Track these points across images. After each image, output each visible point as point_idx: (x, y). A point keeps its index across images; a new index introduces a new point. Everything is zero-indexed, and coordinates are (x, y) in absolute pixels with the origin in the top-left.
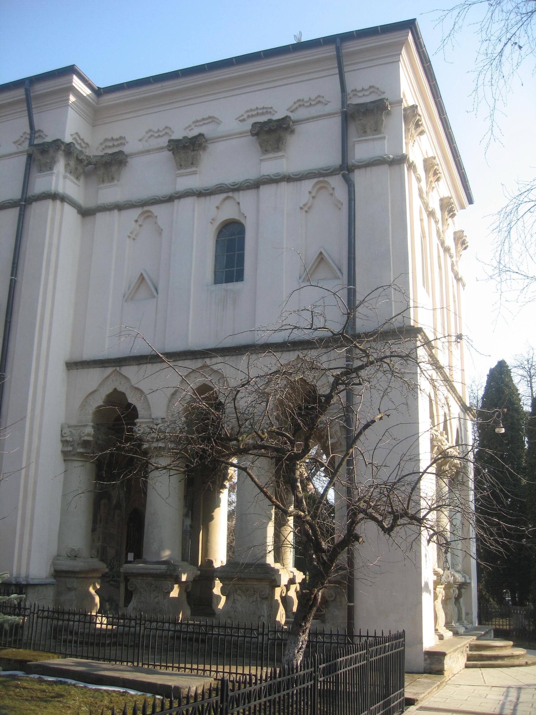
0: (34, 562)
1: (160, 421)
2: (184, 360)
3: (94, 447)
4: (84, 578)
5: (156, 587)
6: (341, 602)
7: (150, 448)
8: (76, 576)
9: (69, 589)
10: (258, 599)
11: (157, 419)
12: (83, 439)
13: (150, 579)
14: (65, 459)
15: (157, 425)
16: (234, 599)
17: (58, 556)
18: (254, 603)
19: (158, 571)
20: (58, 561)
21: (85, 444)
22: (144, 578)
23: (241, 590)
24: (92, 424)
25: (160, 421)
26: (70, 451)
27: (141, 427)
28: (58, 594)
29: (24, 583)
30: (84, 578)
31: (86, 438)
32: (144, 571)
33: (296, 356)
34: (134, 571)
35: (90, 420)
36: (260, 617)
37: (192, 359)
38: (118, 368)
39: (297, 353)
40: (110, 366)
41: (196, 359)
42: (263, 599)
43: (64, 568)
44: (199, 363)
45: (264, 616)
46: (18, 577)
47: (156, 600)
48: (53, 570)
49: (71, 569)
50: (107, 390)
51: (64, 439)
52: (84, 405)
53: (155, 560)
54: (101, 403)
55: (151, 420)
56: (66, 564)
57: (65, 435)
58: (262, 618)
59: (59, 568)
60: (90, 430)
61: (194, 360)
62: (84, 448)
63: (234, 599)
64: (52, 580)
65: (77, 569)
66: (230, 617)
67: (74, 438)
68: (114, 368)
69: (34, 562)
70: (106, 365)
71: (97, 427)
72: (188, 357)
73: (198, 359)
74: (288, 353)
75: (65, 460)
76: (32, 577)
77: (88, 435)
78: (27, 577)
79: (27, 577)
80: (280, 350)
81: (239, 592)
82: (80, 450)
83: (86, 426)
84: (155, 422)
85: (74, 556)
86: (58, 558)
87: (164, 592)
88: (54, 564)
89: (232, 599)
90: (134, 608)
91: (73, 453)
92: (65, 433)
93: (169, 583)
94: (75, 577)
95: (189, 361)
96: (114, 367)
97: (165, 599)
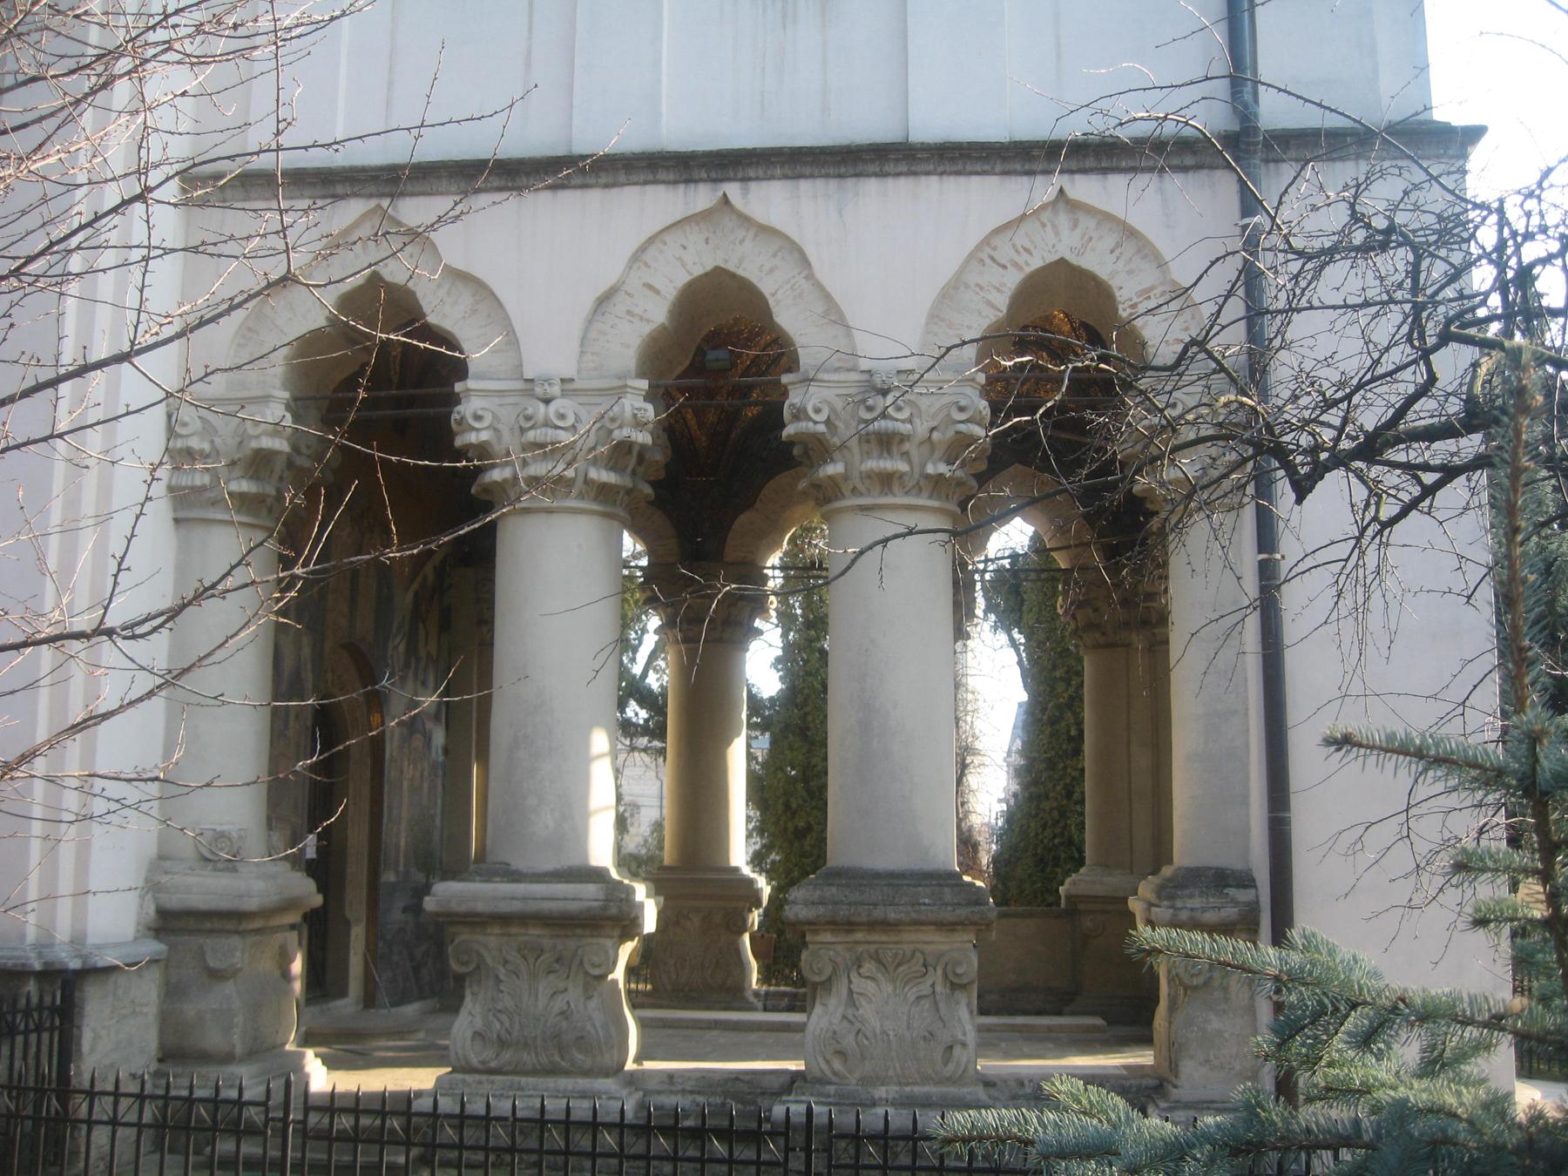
0: (89, 892)
1: (556, 390)
2: (645, 183)
3: (281, 478)
4: (258, 931)
5: (558, 960)
6: (1225, 989)
7: (846, 477)
8: (242, 928)
9: (217, 975)
10: (939, 988)
11: (548, 381)
12: (254, 444)
13: (535, 931)
14: (181, 515)
15: (547, 401)
16: (851, 992)
17: (162, 857)
18: (926, 1004)
19: (573, 907)
20: (167, 878)
21: (259, 462)
22: (514, 930)
23: (879, 961)
24: (287, 395)
25: (556, 390)
26: (203, 488)
27: (482, 413)
28: (172, 991)
29: (75, 964)
30: (258, 931)
31: (267, 443)
32: (516, 906)
33: (1052, 192)
34: (480, 907)
35: (278, 382)
36: (951, 1047)
37: (676, 182)
38: (385, 203)
39: (1057, 180)
40: (356, 195)
41: (687, 181)
42: (954, 987)
43: (197, 901)
44: (702, 197)
45: (964, 1045)
46: (42, 946)
47: (559, 1004)
48: (152, 910)
49: (225, 905)
50: (351, 270)
51: (179, 444)
52: (250, 329)
53: (549, 864)
54: (318, 320)
55: (519, 385)
56: (204, 889)
57: (183, 431)
58: (957, 1050)
59: (175, 901)
60: (276, 412)
61: (682, 187)
62: (251, 478)
63: (851, 992)
64: (154, 947)
65: (251, 904)
66: (841, 1053)
67: (218, 441)
68: (373, 203)
69: (89, 892)
70: (340, 190)
71: (297, 406)
72: (662, 175)
73: (696, 181)
74: (1025, 179)
75: (177, 521)
76: (97, 941)
77: (639, 424)
78: (78, 940)
79: (78, 940)
80: (998, 168)
81: (869, 967)
82: (245, 486)
83: (265, 399)
84: (539, 390)
85: (218, 855)
86: (167, 864)
87: (587, 973)
88: (152, 886)
89: (844, 991)
90: (477, 1035)
91: (208, 494)
92: (185, 425)
93: (609, 943)
94: (237, 932)
95: (661, 188)
96: (371, 196)
97: (590, 998)
